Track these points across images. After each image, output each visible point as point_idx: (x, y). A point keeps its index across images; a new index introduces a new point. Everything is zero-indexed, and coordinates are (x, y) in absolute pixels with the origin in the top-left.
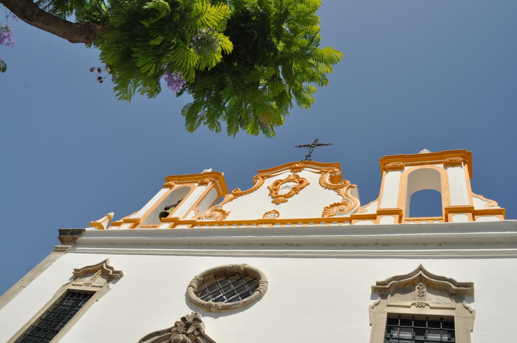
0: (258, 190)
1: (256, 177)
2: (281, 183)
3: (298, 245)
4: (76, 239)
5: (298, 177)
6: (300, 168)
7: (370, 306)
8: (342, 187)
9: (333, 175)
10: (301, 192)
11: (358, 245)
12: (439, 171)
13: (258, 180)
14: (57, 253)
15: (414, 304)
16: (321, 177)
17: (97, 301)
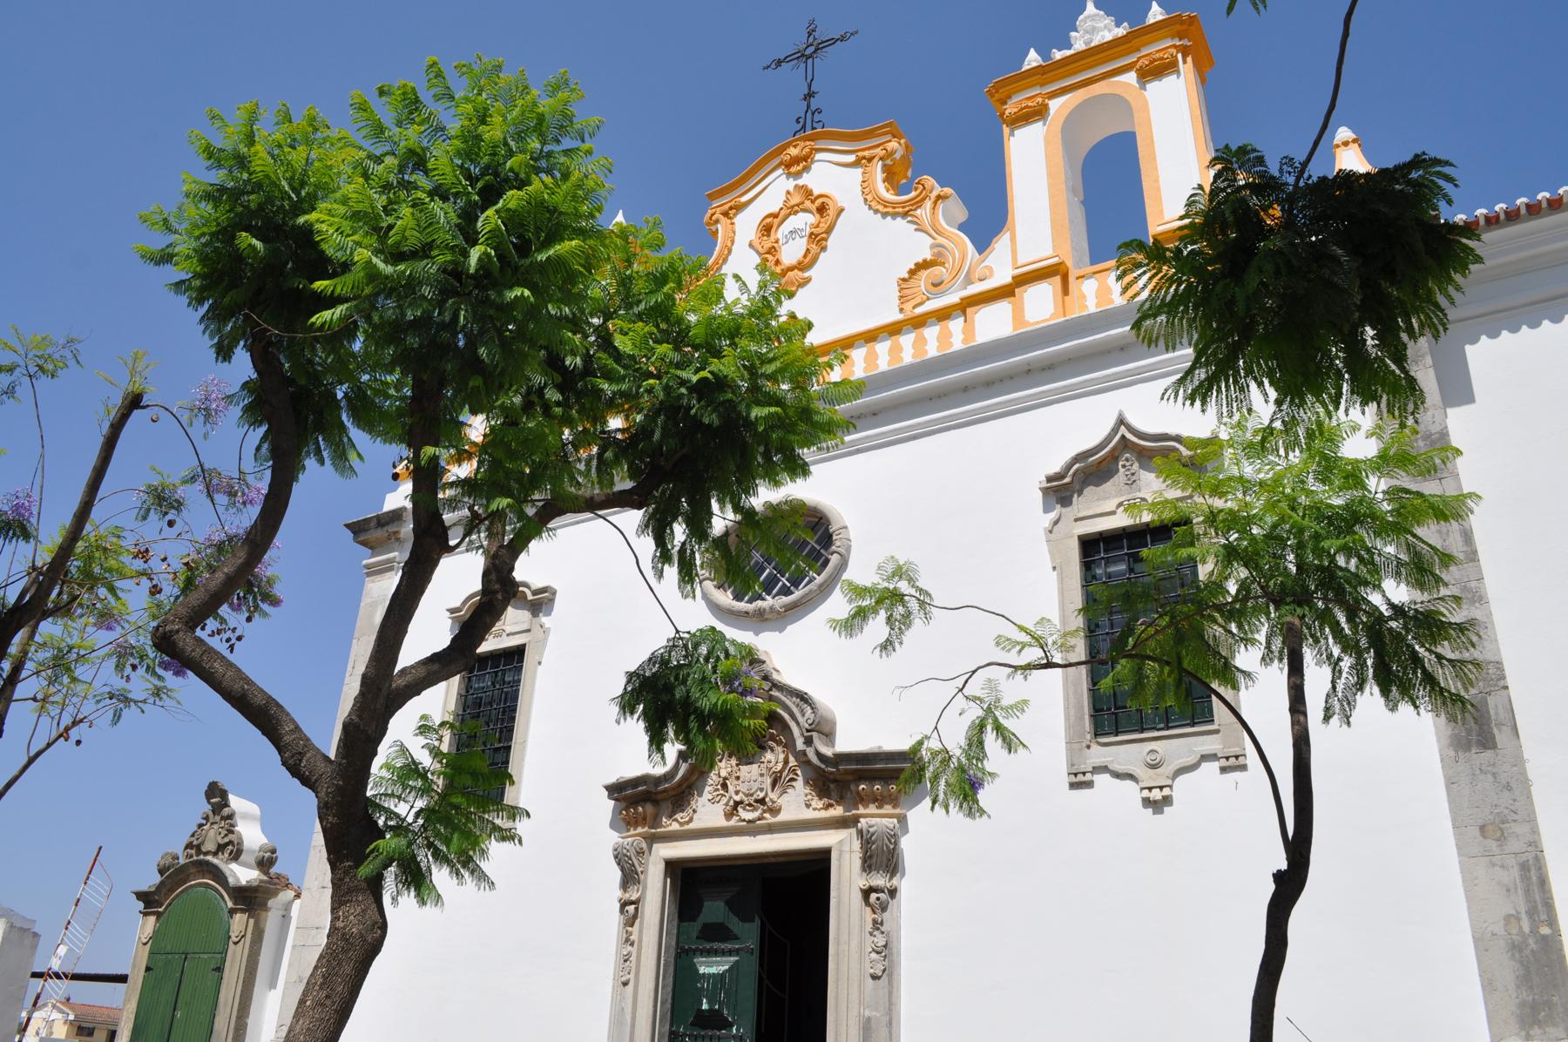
0: (730, 257)
1: (711, 218)
2: (776, 221)
3: (875, 414)
4: (396, 533)
5: (807, 192)
6: (805, 159)
7: (1045, 528)
8: (918, 203)
9: (889, 162)
10: (832, 242)
11: (993, 383)
12: (1129, 99)
13: (719, 226)
14: (378, 578)
15: (1120, 504)
16: (864, 182)
17: (540, 663)
